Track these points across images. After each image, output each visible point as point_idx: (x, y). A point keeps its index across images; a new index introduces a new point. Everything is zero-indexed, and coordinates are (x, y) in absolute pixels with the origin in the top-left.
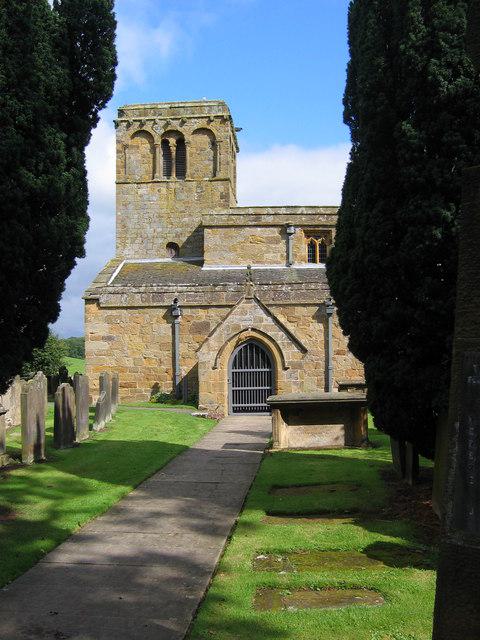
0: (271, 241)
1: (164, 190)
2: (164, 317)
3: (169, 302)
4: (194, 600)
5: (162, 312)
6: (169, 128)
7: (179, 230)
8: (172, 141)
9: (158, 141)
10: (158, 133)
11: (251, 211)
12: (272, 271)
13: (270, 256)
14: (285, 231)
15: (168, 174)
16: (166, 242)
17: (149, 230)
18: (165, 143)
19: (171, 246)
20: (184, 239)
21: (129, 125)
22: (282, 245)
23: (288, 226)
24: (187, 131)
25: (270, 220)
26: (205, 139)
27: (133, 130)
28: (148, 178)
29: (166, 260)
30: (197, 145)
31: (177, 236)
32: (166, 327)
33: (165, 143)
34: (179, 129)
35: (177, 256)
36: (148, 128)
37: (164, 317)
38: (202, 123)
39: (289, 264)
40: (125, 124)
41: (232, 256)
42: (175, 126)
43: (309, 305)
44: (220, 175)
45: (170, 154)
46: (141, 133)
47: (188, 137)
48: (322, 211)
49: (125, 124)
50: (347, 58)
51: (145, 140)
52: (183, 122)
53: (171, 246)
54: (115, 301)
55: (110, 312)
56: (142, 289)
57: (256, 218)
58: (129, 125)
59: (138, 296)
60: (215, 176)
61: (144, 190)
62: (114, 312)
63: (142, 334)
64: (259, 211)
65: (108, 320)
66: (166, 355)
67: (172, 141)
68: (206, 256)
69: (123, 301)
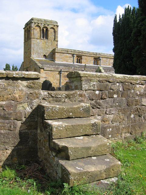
0: (70, 57)
1: (43, 41)
2: (58, 73)
3: (59, 70)
4: (38, 156)
5: (58, 72)
6: (45, 26)
7: (47, 52)
8: (45, 29)
9: (42, 28)
10: (42, 27)
11: (66, 50)
12: (109, 67)
13: (69, 61)
14: (73, 55)
15: (43, 37)
16: (43, 55)
17: (40, 51)
18: (43, 29)
19: (45, 56)
20: (48, 54)
21: (35, 23)
22: (72, 59)
23: (74, 54)
24: (49, 27)
25: (70, 52)
26: (52, 30)
27: (36, 25)
28: (39, 38)
29: (71, 63)
30: (51, 31)
31: (46, 53)
32: (58, 76)
33: (43, 29)
34: (47, 27)
35: (46, 58)
36: (40, 25)
37: (58, 73)
38: (52, 26)
39: (74, 63)
40: (34, 23)
41: (62, 60)
42: (46, 25)
43: (57, 71)
44: (56, 40)
45: (44, 33)
46: (38, 26)
47: (49, 29)
48: (80, 52)
49: (34, 23)
50: (113, 46)
51: (38, 28)
52: (48, 25)
53: (45, 56)
54: (48, 69)
55: (46, 71)
56: (54, 67)
57: (67, 52)
58: (35, 23)
59: (53, 68)
60: (55, 40)
61: (38, 41)
62: (47, 71)
63: (53, 77)
64: (68, 50)
65: (46, 73)
66: (58, 82)
67: (45, 29)
68: (56, 59)
69: (49, 69)
